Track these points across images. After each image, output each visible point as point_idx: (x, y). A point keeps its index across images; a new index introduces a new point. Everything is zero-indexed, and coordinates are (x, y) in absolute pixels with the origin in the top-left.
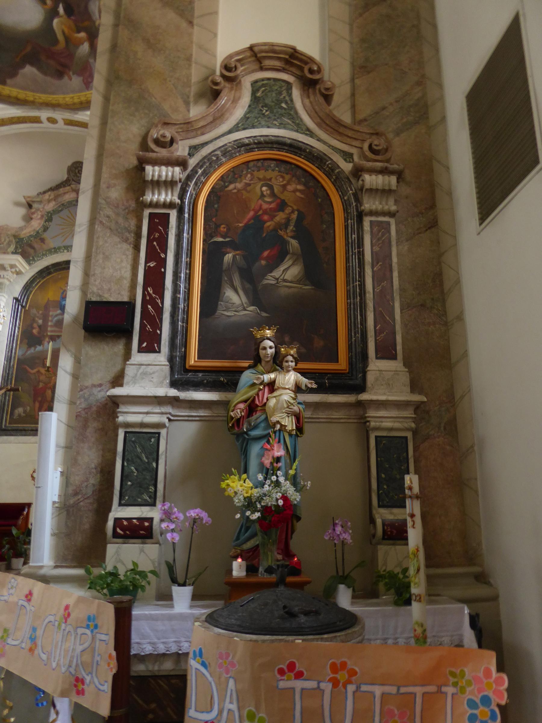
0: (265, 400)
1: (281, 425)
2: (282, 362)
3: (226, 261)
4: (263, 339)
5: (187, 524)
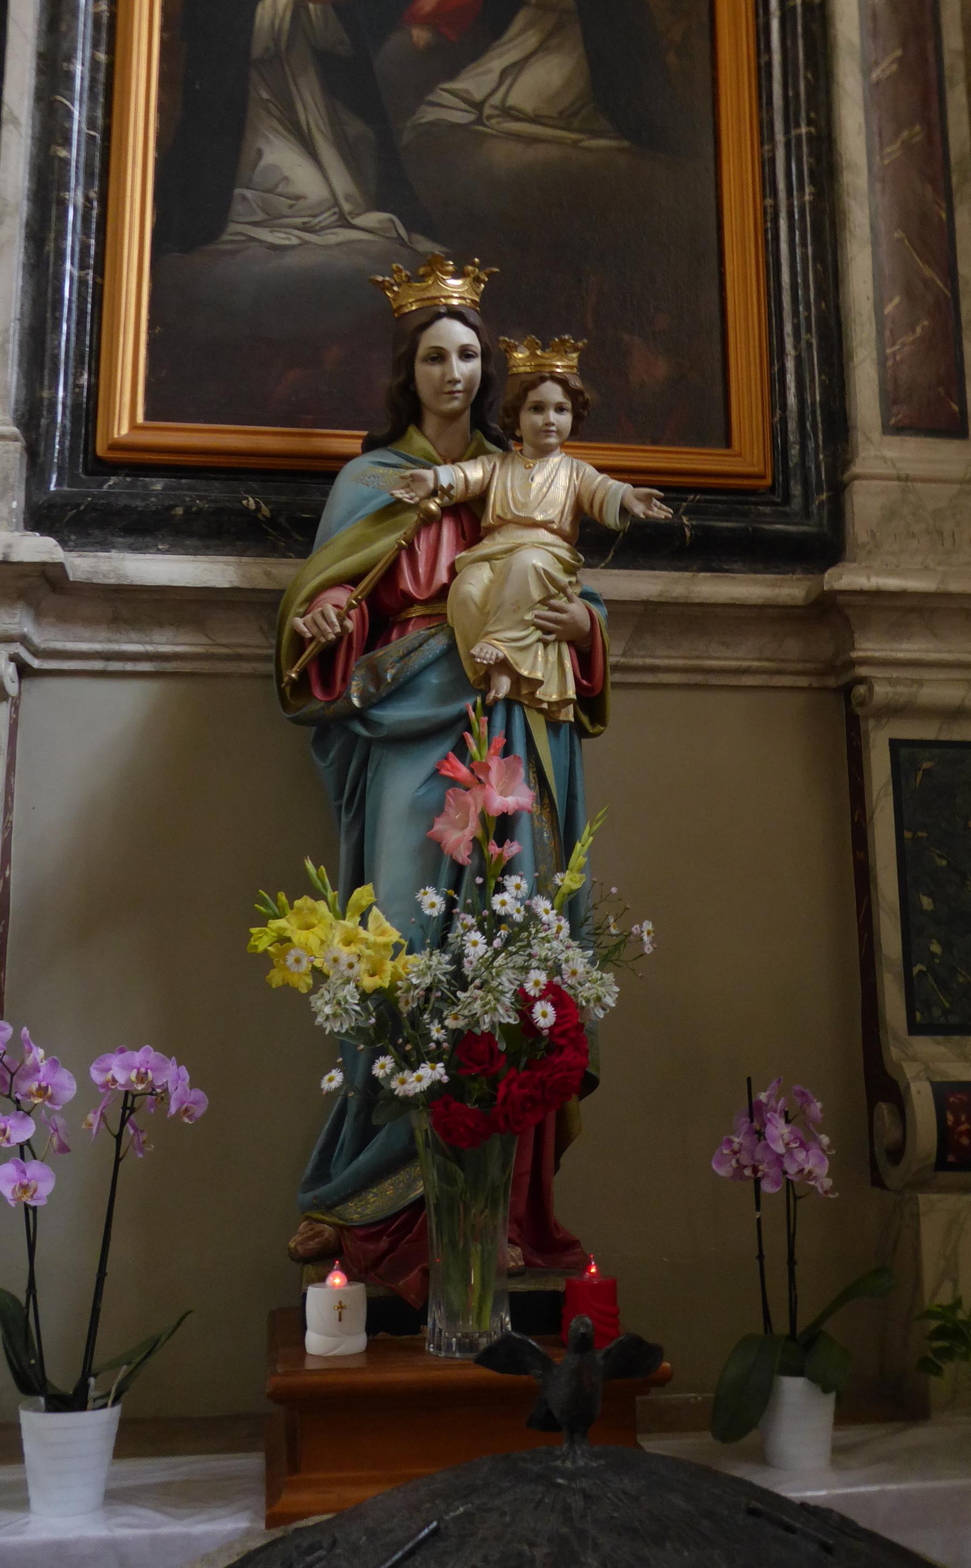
0: (442, 576)
1: (518, 680)
2: (514, 412)
3: (267, 22)
4: (436, 312)
5: (93, 1118)
